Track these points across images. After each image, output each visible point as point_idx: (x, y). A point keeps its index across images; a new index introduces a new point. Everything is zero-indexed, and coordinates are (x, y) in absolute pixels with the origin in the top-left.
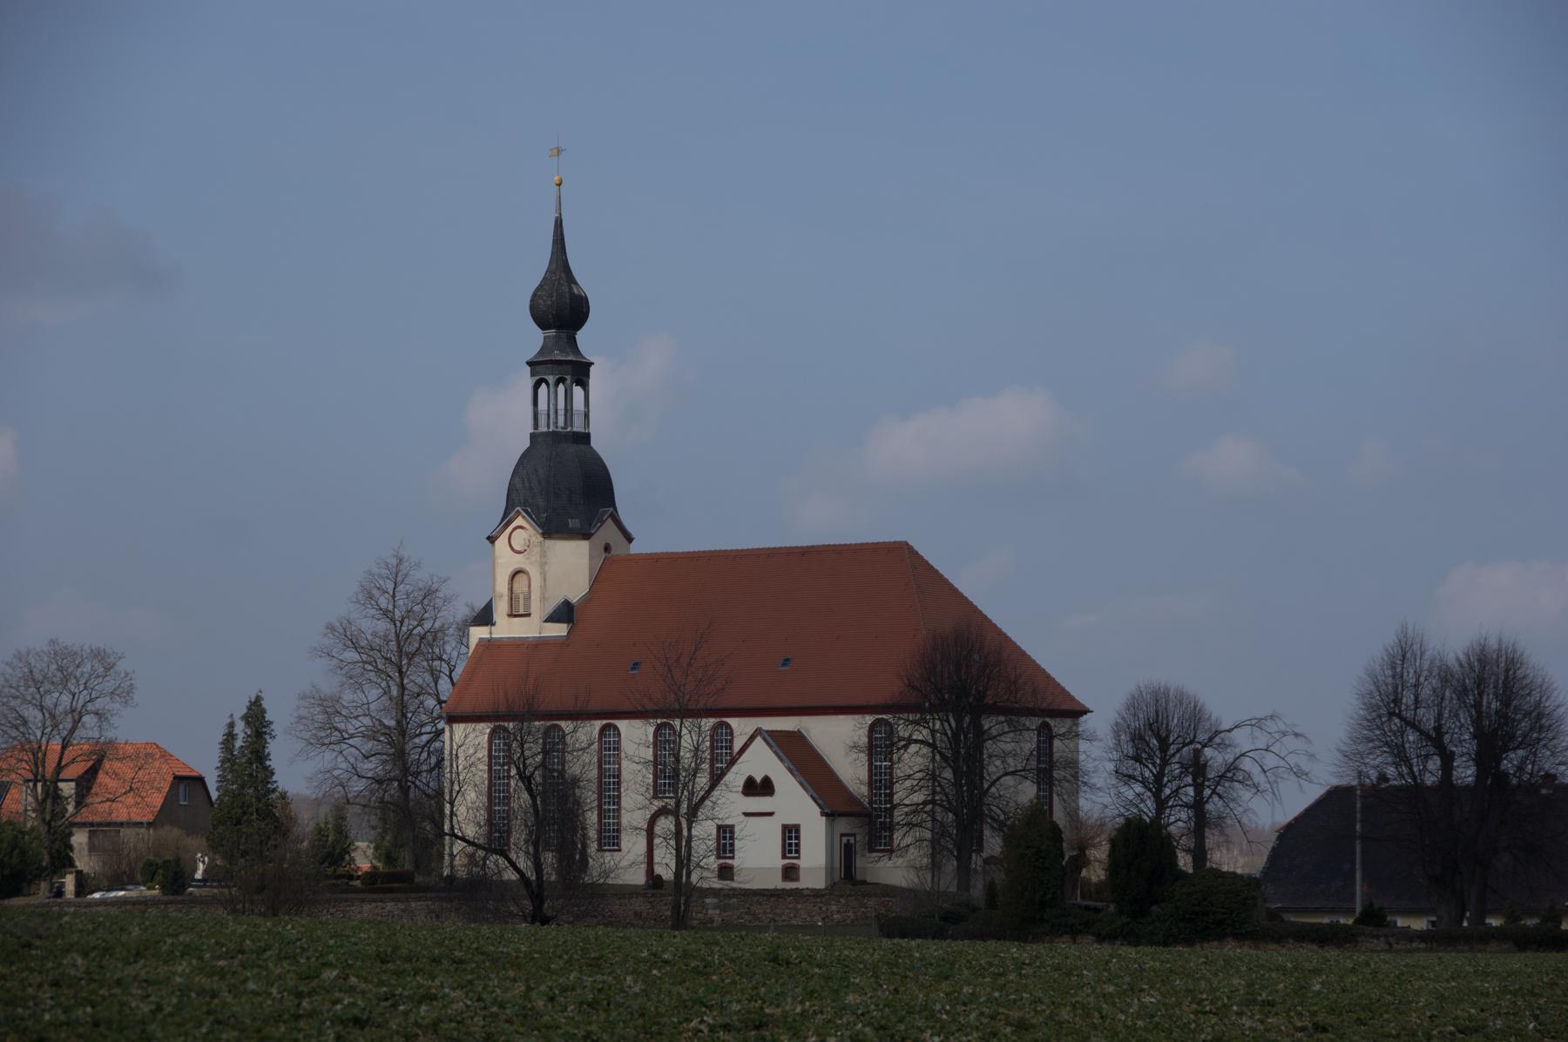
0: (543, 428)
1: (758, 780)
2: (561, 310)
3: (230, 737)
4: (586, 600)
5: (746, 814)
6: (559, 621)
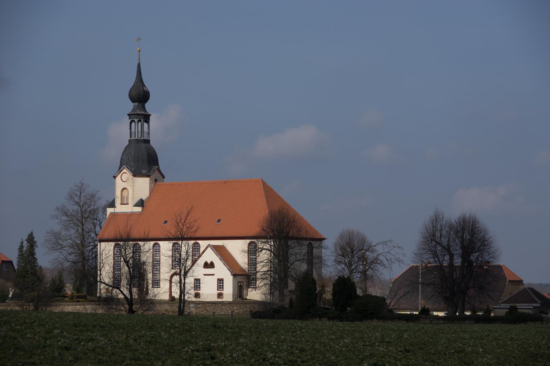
1: (209, 263)
2: (140, 96)
3: (22, 247)
4: (149, 199)
5: (204, 275)
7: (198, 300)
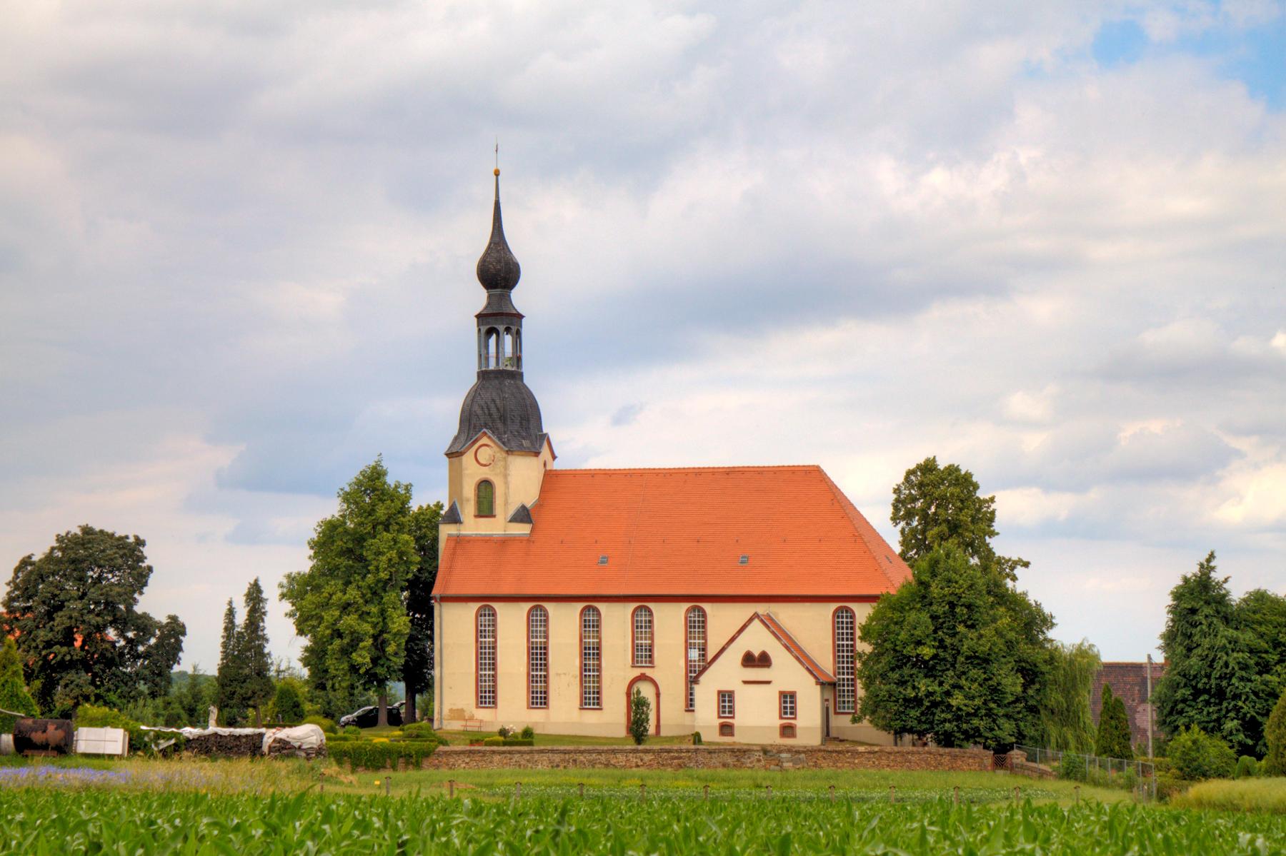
0: (492, 366)
1: (756, 654)
2: (498, 273)
3: (231, 613)
4: (540, 504)
5: (745, 682)
7: (789, 742)
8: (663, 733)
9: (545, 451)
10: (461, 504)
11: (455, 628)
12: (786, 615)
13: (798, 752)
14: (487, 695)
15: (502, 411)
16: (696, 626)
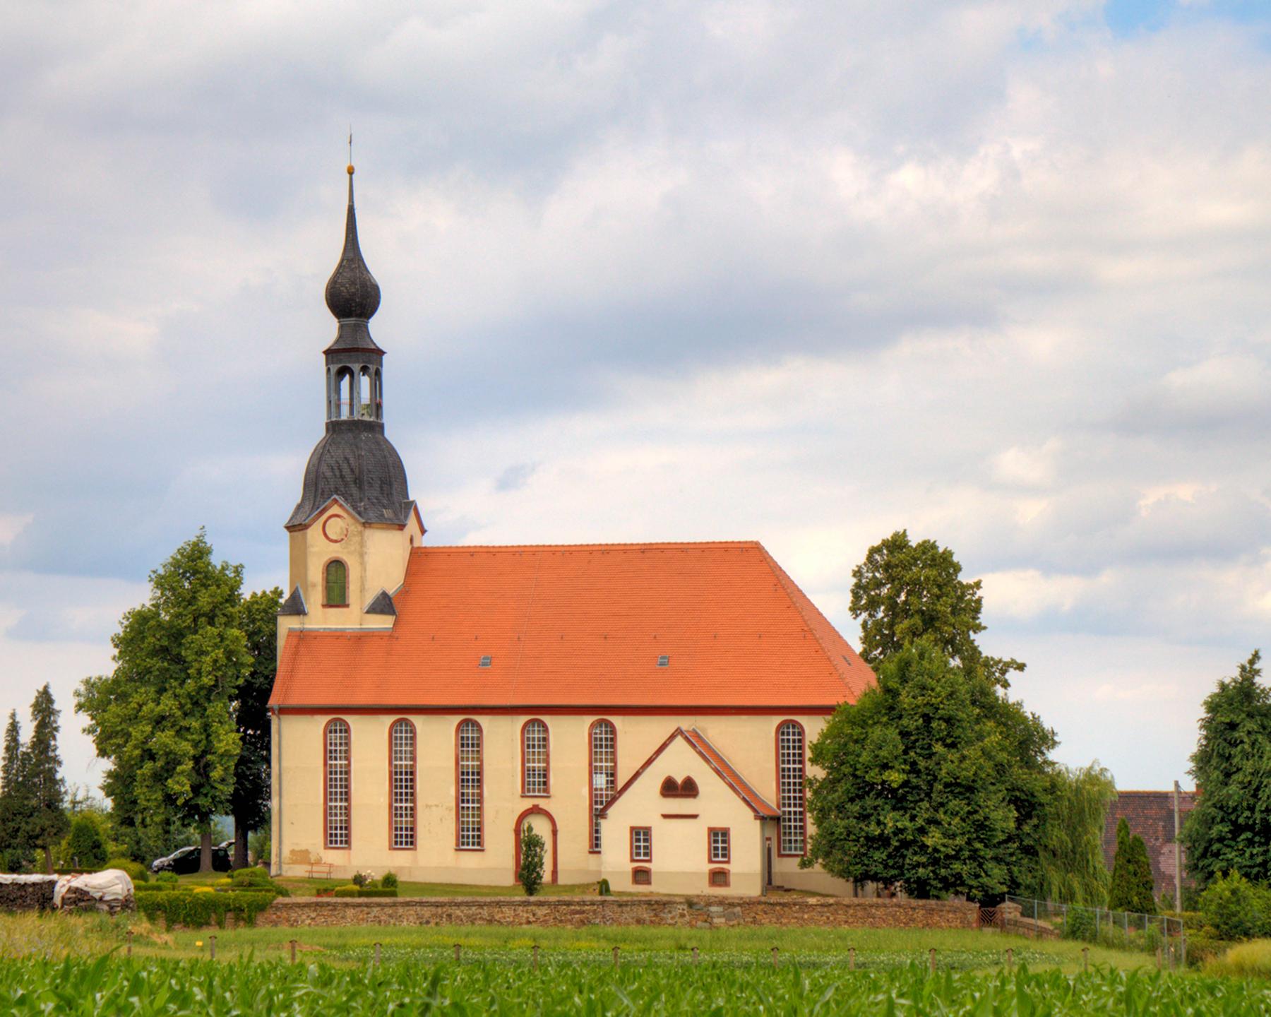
0: (345, 415)
1: (679, 780)
2: (353, 297)
3: (14, 729)
4: (405, 590)
5: (665, 816)
6: (382, 612)
8: (562, 880)
9: (412, 523)
10: (306, 590)
11: (297, 747)
12: (716, 730)
13: (732, 905)
14: (338, 833)
15: (358, 472)
16: (603, 745)
